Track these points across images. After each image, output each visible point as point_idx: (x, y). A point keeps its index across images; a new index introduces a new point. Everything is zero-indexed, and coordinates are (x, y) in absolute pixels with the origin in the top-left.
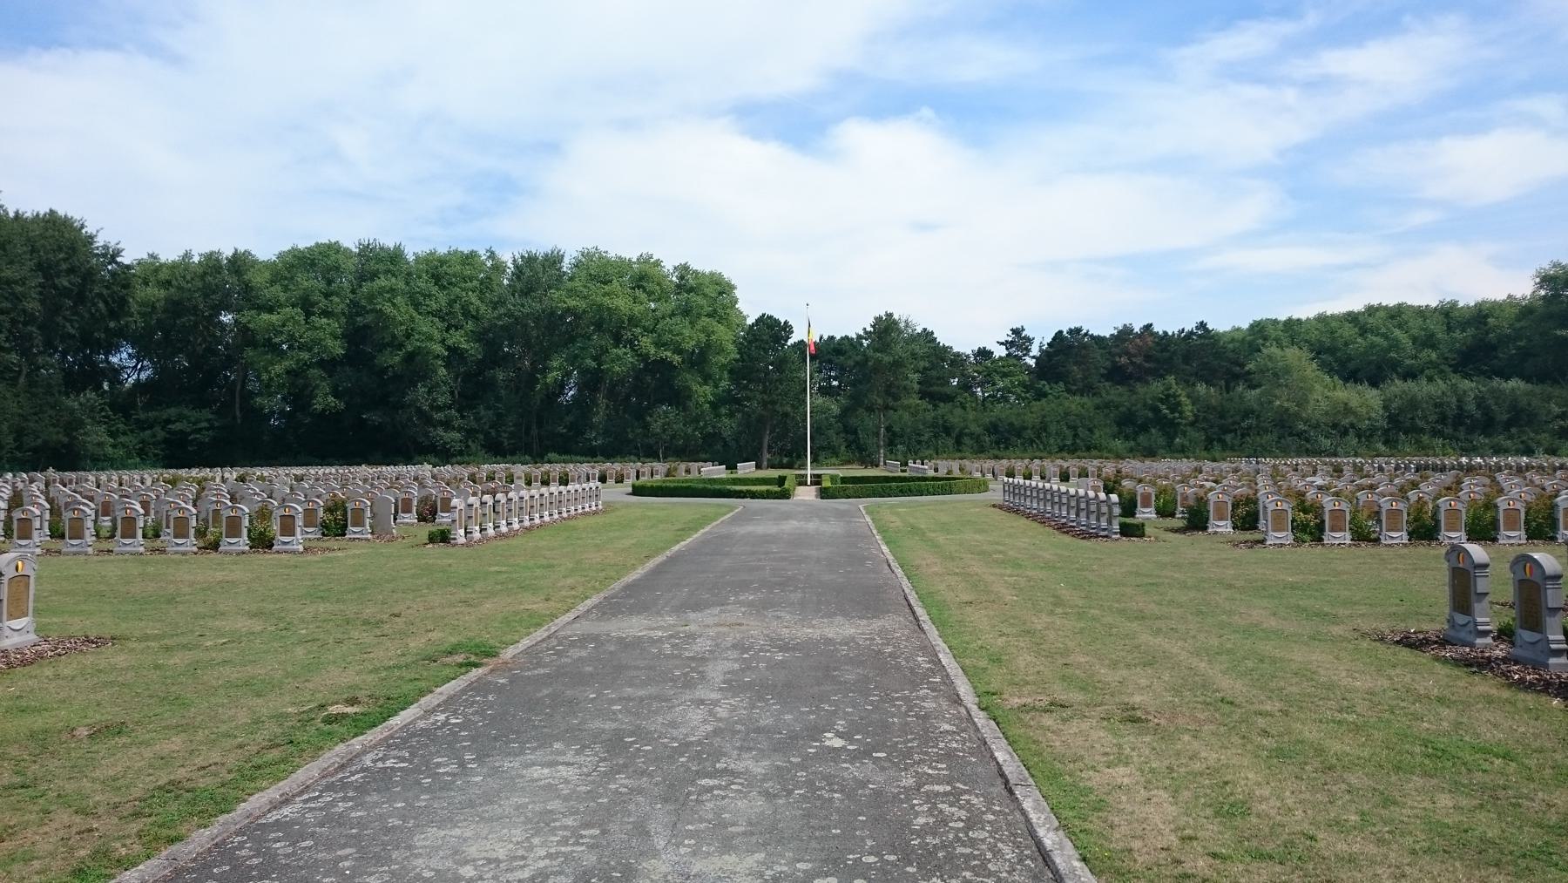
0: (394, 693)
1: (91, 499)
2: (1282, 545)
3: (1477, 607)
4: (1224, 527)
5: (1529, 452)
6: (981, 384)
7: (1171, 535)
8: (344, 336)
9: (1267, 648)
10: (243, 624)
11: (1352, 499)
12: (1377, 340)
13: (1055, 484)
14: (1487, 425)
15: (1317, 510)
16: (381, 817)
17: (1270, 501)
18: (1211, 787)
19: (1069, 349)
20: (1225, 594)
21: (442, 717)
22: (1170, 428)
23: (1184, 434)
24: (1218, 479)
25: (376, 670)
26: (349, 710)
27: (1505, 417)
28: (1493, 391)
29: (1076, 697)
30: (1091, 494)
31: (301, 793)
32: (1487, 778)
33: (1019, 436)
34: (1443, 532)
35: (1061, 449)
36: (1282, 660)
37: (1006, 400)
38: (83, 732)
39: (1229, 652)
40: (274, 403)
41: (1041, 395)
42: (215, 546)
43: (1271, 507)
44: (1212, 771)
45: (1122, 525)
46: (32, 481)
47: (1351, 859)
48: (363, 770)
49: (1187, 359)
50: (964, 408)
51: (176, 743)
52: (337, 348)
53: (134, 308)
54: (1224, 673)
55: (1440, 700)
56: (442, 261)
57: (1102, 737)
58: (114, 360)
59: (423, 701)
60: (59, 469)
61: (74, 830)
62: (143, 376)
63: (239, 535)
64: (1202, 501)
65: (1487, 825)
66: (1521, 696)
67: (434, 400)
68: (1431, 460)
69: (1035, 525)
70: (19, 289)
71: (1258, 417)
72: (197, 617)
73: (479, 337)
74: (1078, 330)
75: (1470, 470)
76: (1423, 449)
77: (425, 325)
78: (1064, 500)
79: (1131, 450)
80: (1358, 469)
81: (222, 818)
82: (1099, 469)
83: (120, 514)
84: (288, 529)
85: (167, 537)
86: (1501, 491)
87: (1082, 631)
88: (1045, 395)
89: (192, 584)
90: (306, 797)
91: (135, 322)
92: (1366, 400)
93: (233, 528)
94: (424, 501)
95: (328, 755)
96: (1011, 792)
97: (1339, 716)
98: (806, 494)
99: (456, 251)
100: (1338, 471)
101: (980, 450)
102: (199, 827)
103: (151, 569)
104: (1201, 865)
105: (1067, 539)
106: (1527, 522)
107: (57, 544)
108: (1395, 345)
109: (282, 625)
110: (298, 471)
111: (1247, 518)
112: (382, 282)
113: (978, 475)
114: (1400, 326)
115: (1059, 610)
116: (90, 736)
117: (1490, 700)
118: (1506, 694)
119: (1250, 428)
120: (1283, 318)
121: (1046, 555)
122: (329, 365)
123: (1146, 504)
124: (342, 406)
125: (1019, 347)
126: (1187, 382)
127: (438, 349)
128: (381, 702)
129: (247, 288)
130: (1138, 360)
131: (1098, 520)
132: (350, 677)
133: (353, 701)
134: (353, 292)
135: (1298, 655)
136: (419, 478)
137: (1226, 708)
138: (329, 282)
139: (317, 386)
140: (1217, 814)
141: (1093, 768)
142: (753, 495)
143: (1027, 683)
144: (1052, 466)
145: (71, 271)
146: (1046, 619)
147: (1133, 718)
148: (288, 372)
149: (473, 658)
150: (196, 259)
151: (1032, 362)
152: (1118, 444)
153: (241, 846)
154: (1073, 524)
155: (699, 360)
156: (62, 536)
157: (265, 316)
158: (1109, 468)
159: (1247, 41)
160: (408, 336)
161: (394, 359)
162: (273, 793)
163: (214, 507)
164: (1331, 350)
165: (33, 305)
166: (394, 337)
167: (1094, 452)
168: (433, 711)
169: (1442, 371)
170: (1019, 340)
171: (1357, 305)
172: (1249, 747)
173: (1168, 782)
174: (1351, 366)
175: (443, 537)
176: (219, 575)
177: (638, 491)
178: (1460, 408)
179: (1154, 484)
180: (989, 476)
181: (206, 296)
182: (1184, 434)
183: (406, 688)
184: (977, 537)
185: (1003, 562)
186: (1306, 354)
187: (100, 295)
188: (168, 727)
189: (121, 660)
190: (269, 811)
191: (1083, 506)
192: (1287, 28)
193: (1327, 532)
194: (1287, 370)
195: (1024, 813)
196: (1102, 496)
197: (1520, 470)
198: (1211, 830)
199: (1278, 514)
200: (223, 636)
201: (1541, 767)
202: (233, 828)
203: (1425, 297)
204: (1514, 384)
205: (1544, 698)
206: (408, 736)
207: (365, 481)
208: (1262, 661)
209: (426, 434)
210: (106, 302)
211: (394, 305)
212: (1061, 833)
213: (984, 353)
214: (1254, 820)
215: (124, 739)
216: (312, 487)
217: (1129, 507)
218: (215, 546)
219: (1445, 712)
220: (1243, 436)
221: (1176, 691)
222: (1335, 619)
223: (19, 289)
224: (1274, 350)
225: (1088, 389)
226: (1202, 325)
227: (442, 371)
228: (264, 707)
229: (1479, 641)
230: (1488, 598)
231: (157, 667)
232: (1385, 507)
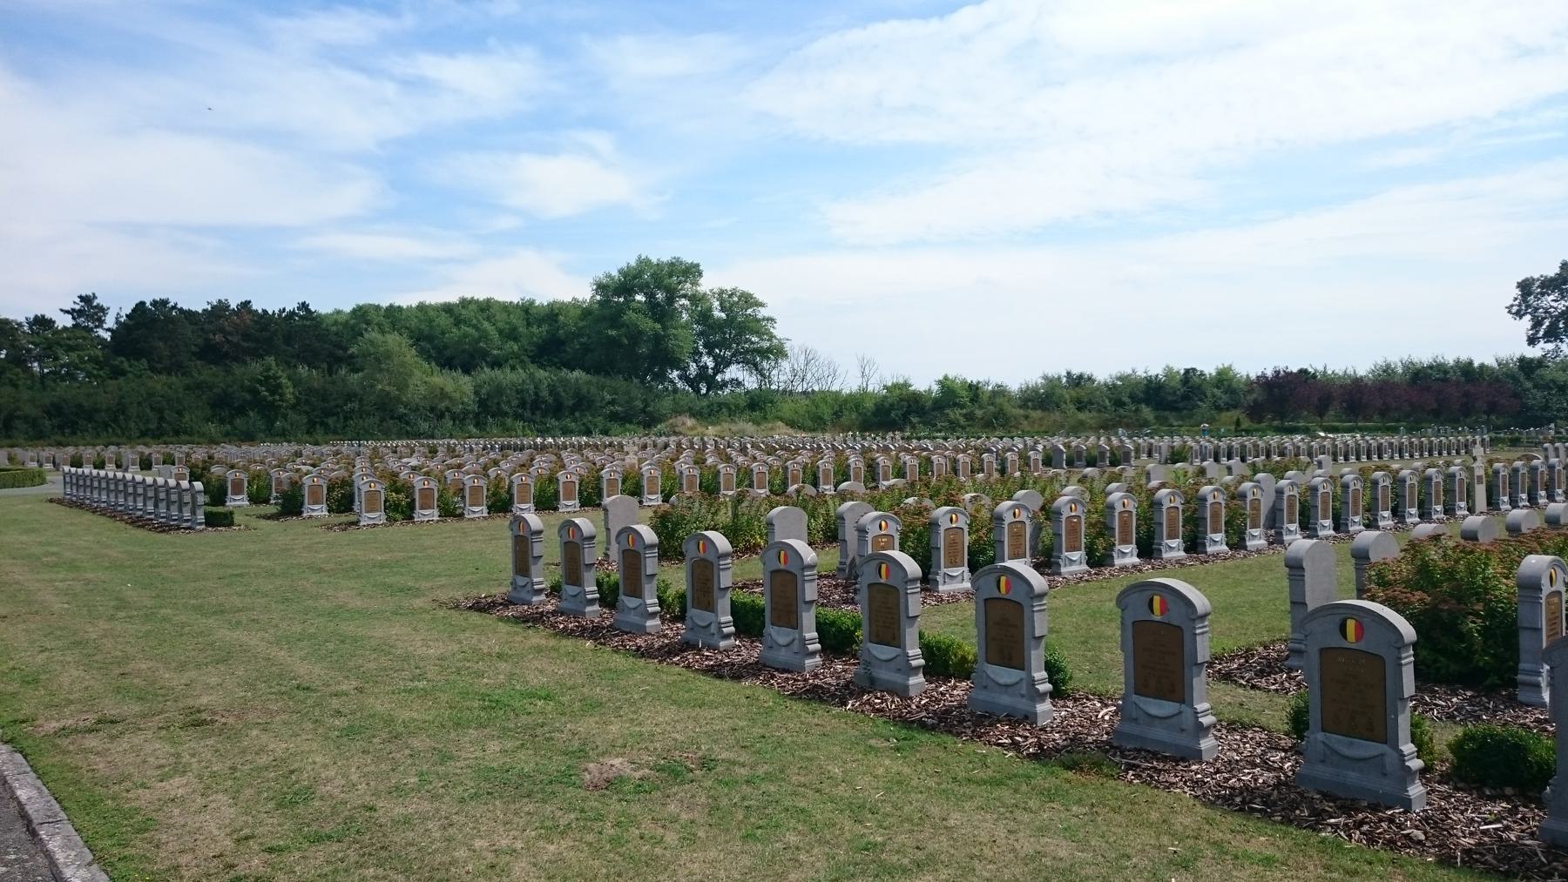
2: (375, 525)
3: (534, 569)
4: (320, 511)
5: (588, 433)
6: (39, 359)
7: (263, 522)
9: (348, 628)
11: (442, 479)
12: (471, 331)
13: (134, 474)
14: (557, 410)
15: (408, 489)
17: (364, 483)
18: (276, 780)
19: (152, 322)
20: (314, 578)
22: (269, 411)
23: (285, 417)
24: (311, 463)
27: (571, 403)
28: (561, 381)
29: (132, 708)
30: (172, 482)
32: (530, 719)
33: (90, 419)
34: (516, 505)
35: (143, 434)
36: (363, 638)
37: (73, 377)
39: (312, 636)
41: (118, 373)
43: (365, 488)
44: (277, 763)
45: (208, 515)
47: (407, 821)
49: (288, 339)
50: (16, 386)
54: (303, 659)
55: (500, 656)
57: (158, 749)
64: (296, 486)
65: (526, 762)
66: (564, 642)
68: (513, 441)
69: (103, 520)
71: (361, 400)
74: (164, 303)
75: (543, 448)
76: (507, 431)
78: (140, 491)
79: (227, 434)
80: (451, 451)
82: (188, 455)
86: (563, 467)
87: (147, 634)
88: (123, 373)
92: (460, 386)
96: (33, 833)
97: (411, 685)
100: (433, 451)
101: (37, 435)
104: (255, 864)
105: (141, 534)
106: (580, 493)
108: (484, 336)
111: (342, 500)
113: (35, 465)
114: (488, 319)
115: (122, 614)
117: (539, 650)
118: (552, 642)
119: (352, 411)
120: (385, 304)
121: (113, 553)
123: (238, 489)
125: (90, 317)
126: (288, 363)
130: (235, 339)
131: (180, 511)
135: (379, 631)
137: (301, 694)
140: (280, 806)
141: (143, 786)
143: (71, 702)
144: (129, 453)
146: (104, 625)
147: (197, 722)
151: (107, 336)
152: (212, 428)
154: (150, 516)
158: (199, 454)
159: (348, 27)
164: (430, 338)
167: (184, 437)
169: (522, 361)
170: (89, 309)
171: (453, 298)
172: (320, 730)
173: (230, 783)
174: (448, 353)
178: (536, 394)
179: (246, 469)
180: (49, 466)
182: (285, 417)
184: (24, 538)
185: (55, 565)
186: (405, 341)
191: (162, 496)
192: (386, 24)
193: (418, 510)
194: (388, 356)
195: (48, 855)
196: (185, 484)
197: (580, 448)
198: (273, 826)
199: (372, 495)
201: (572, 701)
203: (508, 294)
204: (577, 374)
205: (580, 642)
208: (343, 642)
212: (95, 866)
213: (42, 323)
214: (317, 804)
217: (217, 494)
219: (502, 666)
220: (346, 419)
221: (251, 686)
222: (416, 593)
224: (374, 335)
225: (176, 368)
226: (304, 306)
229: (535, 599)
230: (542, 561)
232: (469, 484)
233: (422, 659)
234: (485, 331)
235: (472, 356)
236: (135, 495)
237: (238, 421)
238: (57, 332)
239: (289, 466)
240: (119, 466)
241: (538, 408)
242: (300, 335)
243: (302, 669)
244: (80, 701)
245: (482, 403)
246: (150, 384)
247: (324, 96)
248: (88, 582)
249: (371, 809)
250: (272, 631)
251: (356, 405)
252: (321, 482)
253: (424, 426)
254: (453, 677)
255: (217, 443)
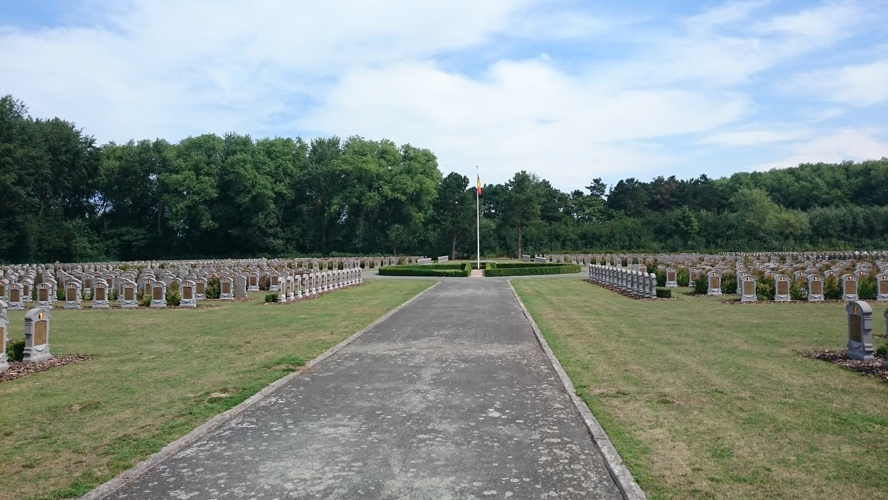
0: (247, 386)
1: (80, 278)
3: (865, 337)
4: (717, 292)
6: (576, 211)
8: (218, 187)
9: (742, 361)
10: (164, 348)
11: (791, 275)
15: (771, 282)
16: (241, 455)
17: (743, 277)
19: (627, 191)
21: (274, 400)
22: (685, 235)
23: (693, 239)
24: (713, 265)
25: (237, 373)
26: (223, 395)
29: (632, 389)
30: (640, 273)
31: (196, 442)
32: (871, 436)
33: (598, 241)
35: (622, 248)
37: (591, 220)
38: (76, 407)
39: (720, 363)
40: (179, 224)
41: (611, 217)
42: (148, 304)
43: (744, 280)
44: (710, 431)
45: (658, 291)
46: (47, 269)
47: (792, 482)
48: (230, 429)
49: (695, 195)
51: (128, 414)
52: (214, 193)
53: (102, 171)
54: (717, 375)
55: (844, 391)
56: (272, 144)
57: (647, 412)
58: (91, 201)
59: (263, 390)
60: (61, 262)
61: (72, 462)
62: (107, 210)
63: (160, 298)
64: (704, 277)
67: (268, 222)
68: (837, 253)
69: (608, 291)
70: (39, 162)
71: (736, 229)
72: (138, 343)
73: (292, 186)
74: (632, 180)
75: (860, 258)
76: (833, 247)
77: (263, 180)
79: (663, 248)
81: (153, 455)
82: (645, 259)
83: (96, 287)
84: (188, 294)
85: (122, 298)
87: (635, 351)
88: (613, 217)
89: (135, 325)
90: (199, 444)
91: (103, 179)
92: (800, 219)
93: (158, 294)
94: (262, 278)
95: (211, 420)
96: (595, 443)
97: (784, 400)
98: (477, 274)
99: (279, 139)
100: (783, 259)
101: (576, 249)
102: (141, 460)
103: (113, 317)
105: (626, 299)
107: (62, 303)
108: (816, 187)
109: (185, 348)
110: (193, 262)
111: (730, 286)
112: (239, 156)
113: (575, 263)
114: (819, 176)
115: (622, 340)
116: (80, 410)
117: (872, 391)
119: (731, 235)
120: (751, 172)
121: (614, 308)
122: (210, 203)
123: (672, 279)
124: (217, 226)
125: (598, 190)
126: (695, 209)
127: (271, 194)
128: (240, 391)
129: (164, 160)
130: (666, 197)
131: (644, 288)
132: (223, 377)
133: (224, 391)
134: (223, 162)
135: (760, 365)
136: (260, 265)
137: (719, 395)
138: (209, 157)
139: (203, 215)
140: (714, 456)
141: (642, 429)
142: (447, 275)
143: (604, 381)
144: (618, 257)
145: (67, 152)
147: (664, 401)
148: (187, 207)
149: (291, 367)
150: (136, 144)
151: (605, 198)
152: (655, 245)
153: (164, 471)
155: (416, 199)
156: (64, 299)
157: (174, 176)
158: (650, 259)
160: (253, 186)
161: (245, 199)
162: (181, 441)
163: (147, 282)
164: (779, 190)
165: (47, 171)
166: (245, 187)
167: (642, 250)
168: (269, 396)
169: (843, 202)
170: (598, 186)
174: (791, 198)
175: (274, 299)
176: (150, 320)
177: (382, 273)
178: (854, 223)
180: (581, 263)
181: (142, 165)
182: (693, 239)
183: (254, 383)
184: (575, 298)
185: (589, 312)
186: (764, 193)
187: (83, 165)
188: (123, 405)
189: (97, 367)
190: (179, 451)
191: (635, 280)
193: (777, 294)
194: (753, 202)
195: (602, 455)
196: (646, 274)
199: (748, 285)
200: (152, 354)
202: (159, 461)
206: (255, 411)
207: (230, 267)
208: (739, 368)
209: (264, 242)
210: (87, 169)
211: (245, 169)
212: (624, 466)
213: (578, 194)
214: (735, 460)
215: (99, 412)
216: (201, 271)
217: (662, 281)
218: (148, 304)
219: (846, 398)
220: (727, 239)
221: (690, 386)
222: (782, 345)
223: (39, 162)
224: (745, 190)
225: (638, 214)
226: (704, 176)
227: (272, 206)
228: (176, 393)
229: (866, 357)
230: (871, 332)
231: (117, 371)
233: (790, 386)
234: (817, 184)
235: (807, 200)
236: (622, 279)
237: (669, 241)
238: (584, 198)
239: (698, 266)
240: (612, 264)
241: (855, 232)
242: (703, 194)
243: (717, 380)
244: (607, 381)
245: (815, 229)
246: (626, 222)
247: (712, 55)
248: (605, 322)
249: (768, 470)
250: (698, 357)
251: (733, 231)
252: (718, 275)
253: (776, 243)
254: (812, 399)
255: (658, 253)
